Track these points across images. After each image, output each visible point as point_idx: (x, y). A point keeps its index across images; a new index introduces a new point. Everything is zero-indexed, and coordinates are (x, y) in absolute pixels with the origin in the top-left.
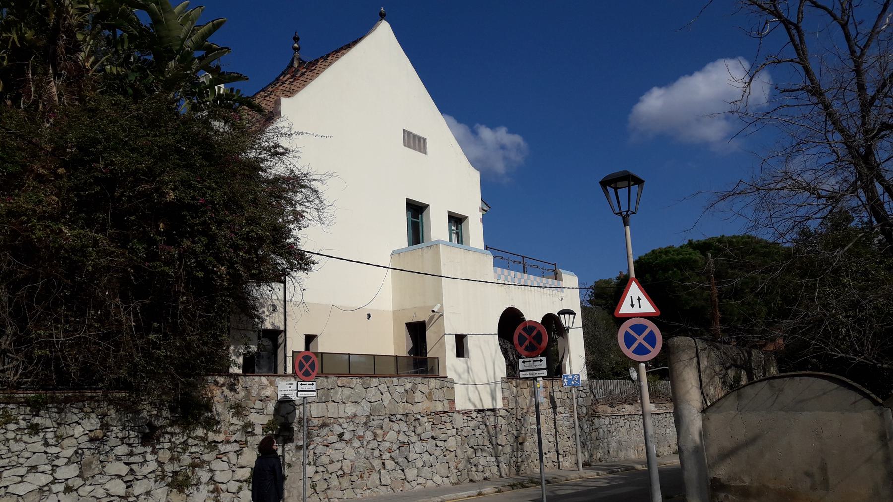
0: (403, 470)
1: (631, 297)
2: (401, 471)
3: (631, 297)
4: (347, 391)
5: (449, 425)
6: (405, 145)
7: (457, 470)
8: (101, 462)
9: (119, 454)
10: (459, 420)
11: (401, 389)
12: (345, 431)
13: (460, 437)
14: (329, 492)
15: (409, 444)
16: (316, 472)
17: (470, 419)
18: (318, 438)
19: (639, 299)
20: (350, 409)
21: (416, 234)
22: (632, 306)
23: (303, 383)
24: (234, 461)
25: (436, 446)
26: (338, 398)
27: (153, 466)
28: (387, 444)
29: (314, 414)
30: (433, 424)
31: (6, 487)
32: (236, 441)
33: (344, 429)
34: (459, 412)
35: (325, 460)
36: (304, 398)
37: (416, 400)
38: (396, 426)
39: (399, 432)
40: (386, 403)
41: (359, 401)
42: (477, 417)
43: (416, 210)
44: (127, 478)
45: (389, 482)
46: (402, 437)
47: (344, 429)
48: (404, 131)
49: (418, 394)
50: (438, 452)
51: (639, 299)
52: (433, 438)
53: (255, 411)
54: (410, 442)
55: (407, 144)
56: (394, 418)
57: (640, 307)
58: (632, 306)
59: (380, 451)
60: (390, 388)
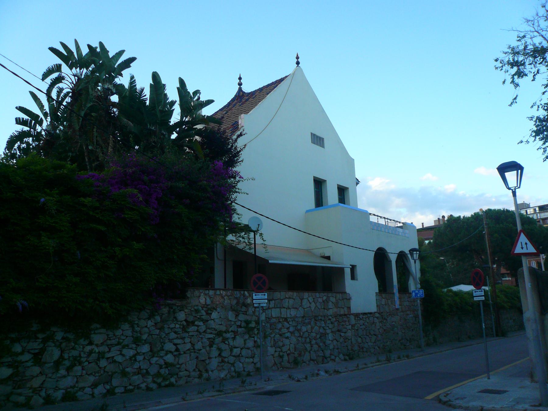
0: (323, 351)
1: (521, 242)
2: (321, 351)
3: (521, 242)
4: (291, 301)
5: (347, 323)
6: (312, 143)
7: (352, 351)
8: (161, 343)
9: (171, 338)
10: (353, 320)
11: (320, 300)
12: (291, 326)
13: (353, 330)
14: (282, 363)
15: (326, 335)
16: (276, 351)
17: (359, 319)
18: (276, 330)
19: (526, 244)
20: (293, 312)
21: (319, 201)
22: (522, 248)
23: (257, 294)
24: (231, 343)
25: (341, 335)
26: (286, 305)
27: (189, 346)
28: (314, 334)
29: (274, 316)
30: (339, 322)
31: (113, 357)
32: (232, 331)
33: (290, 325)
34: (353, 314)
35: (281, 344)
36: (259, 304)
37: (329, 307)
38: (318, 324)
39: (320, 327)
40: (313, 309)
41: (298, 307)
42: (363, 318)
43: (319, 183)
44: (176, 353)
45: (315, 358)
46: (322, 330)
47: (290, 325)
48: (311, 133)
49: (330, 303)
50: (342, 340)
51: (526, 244)
52: (339, 331)
53: (242, 312)
54: (326, 333)
55: (313, 142)
56: (317, 319)
57: (527, 249)
58: (522, 248)
59: (310, 339)
60: (315, 299)
